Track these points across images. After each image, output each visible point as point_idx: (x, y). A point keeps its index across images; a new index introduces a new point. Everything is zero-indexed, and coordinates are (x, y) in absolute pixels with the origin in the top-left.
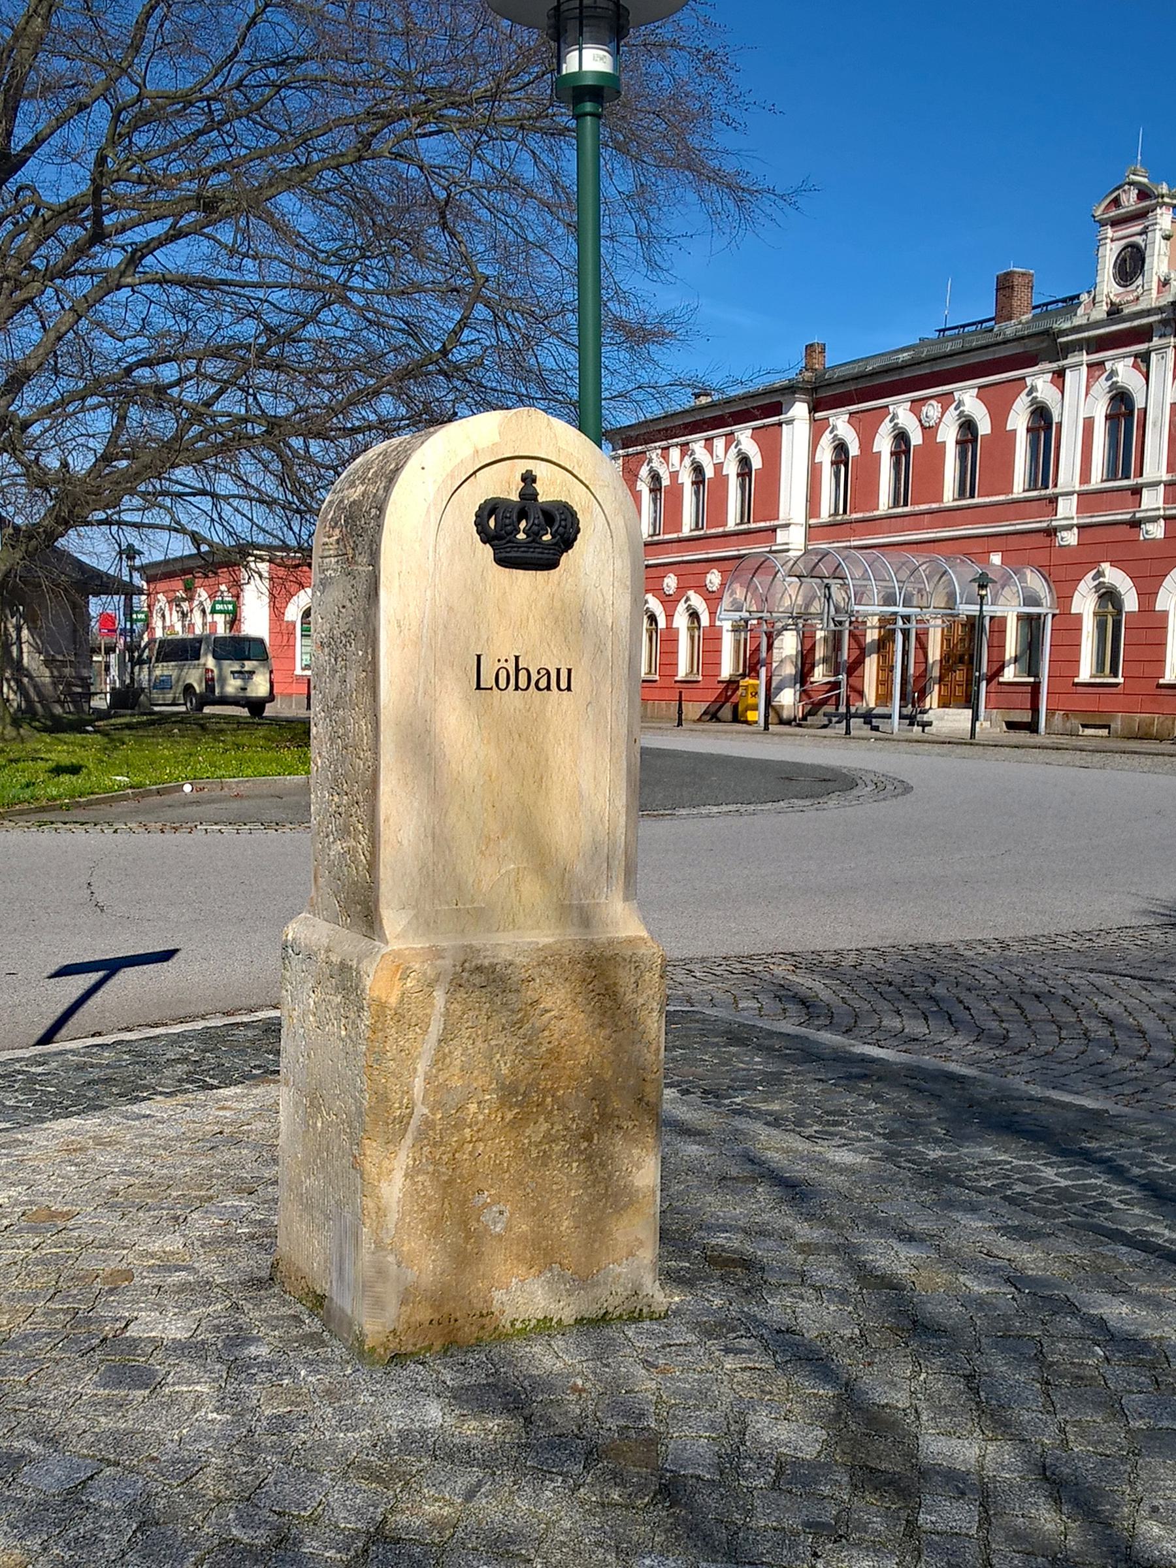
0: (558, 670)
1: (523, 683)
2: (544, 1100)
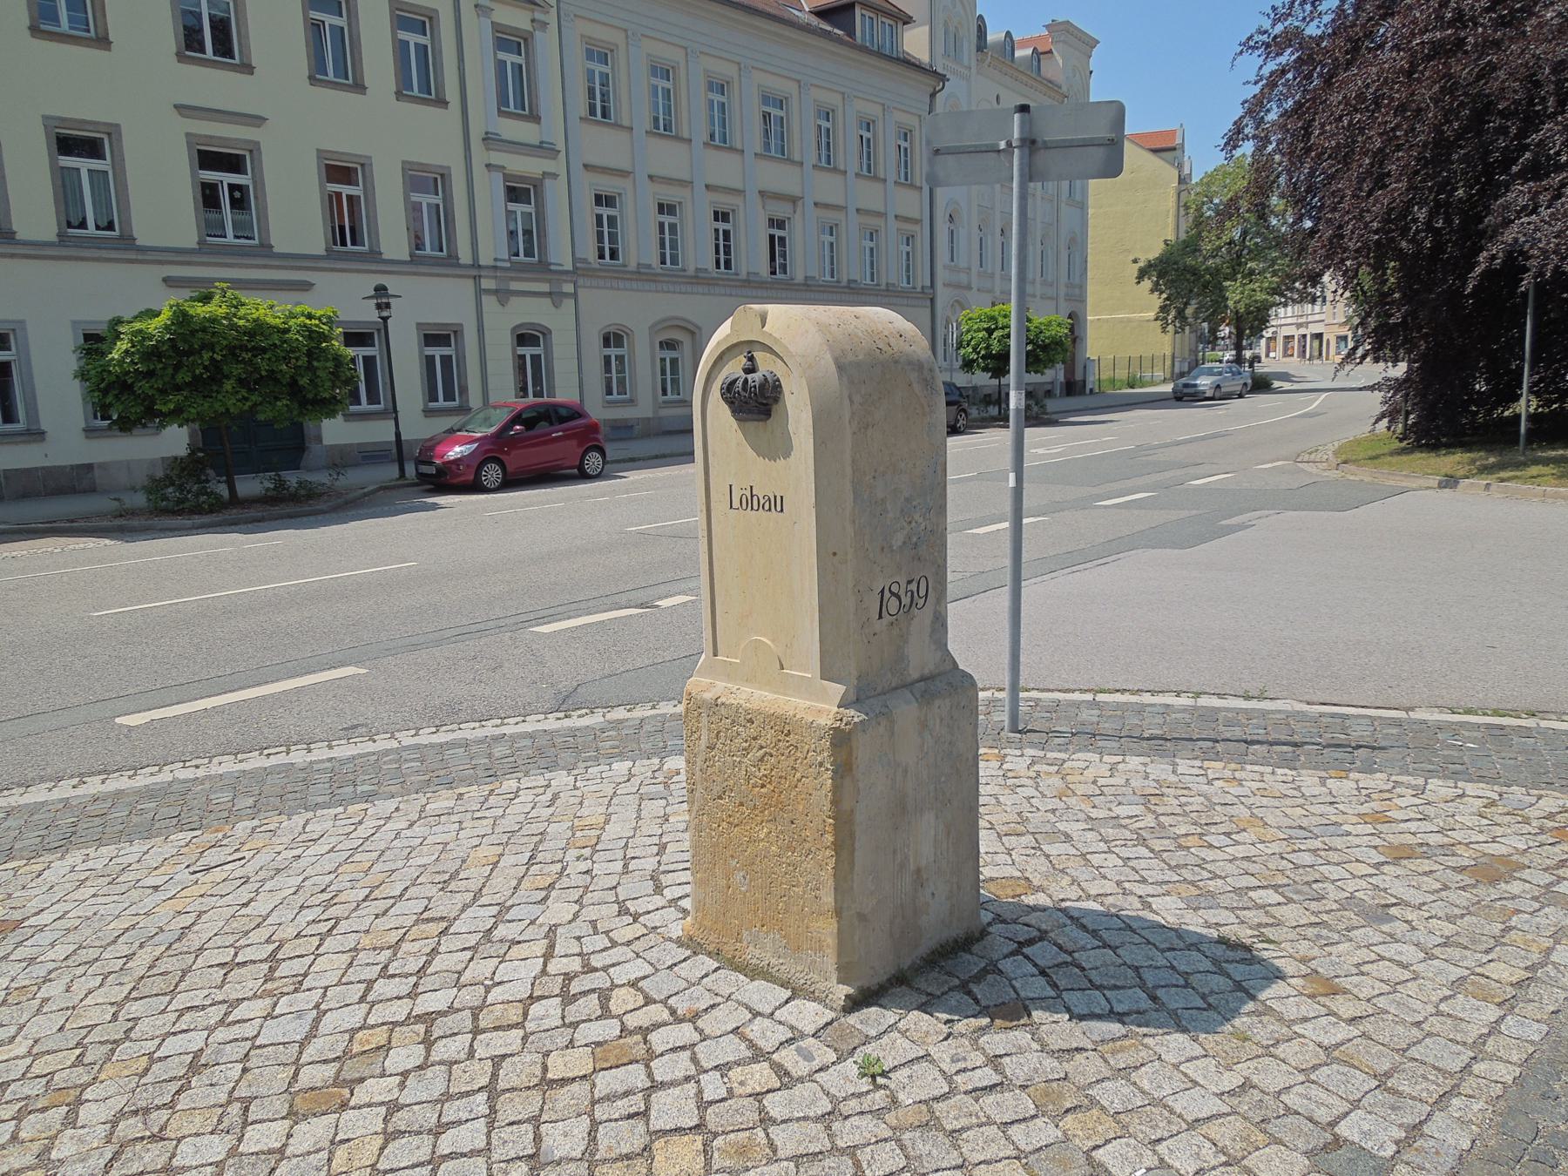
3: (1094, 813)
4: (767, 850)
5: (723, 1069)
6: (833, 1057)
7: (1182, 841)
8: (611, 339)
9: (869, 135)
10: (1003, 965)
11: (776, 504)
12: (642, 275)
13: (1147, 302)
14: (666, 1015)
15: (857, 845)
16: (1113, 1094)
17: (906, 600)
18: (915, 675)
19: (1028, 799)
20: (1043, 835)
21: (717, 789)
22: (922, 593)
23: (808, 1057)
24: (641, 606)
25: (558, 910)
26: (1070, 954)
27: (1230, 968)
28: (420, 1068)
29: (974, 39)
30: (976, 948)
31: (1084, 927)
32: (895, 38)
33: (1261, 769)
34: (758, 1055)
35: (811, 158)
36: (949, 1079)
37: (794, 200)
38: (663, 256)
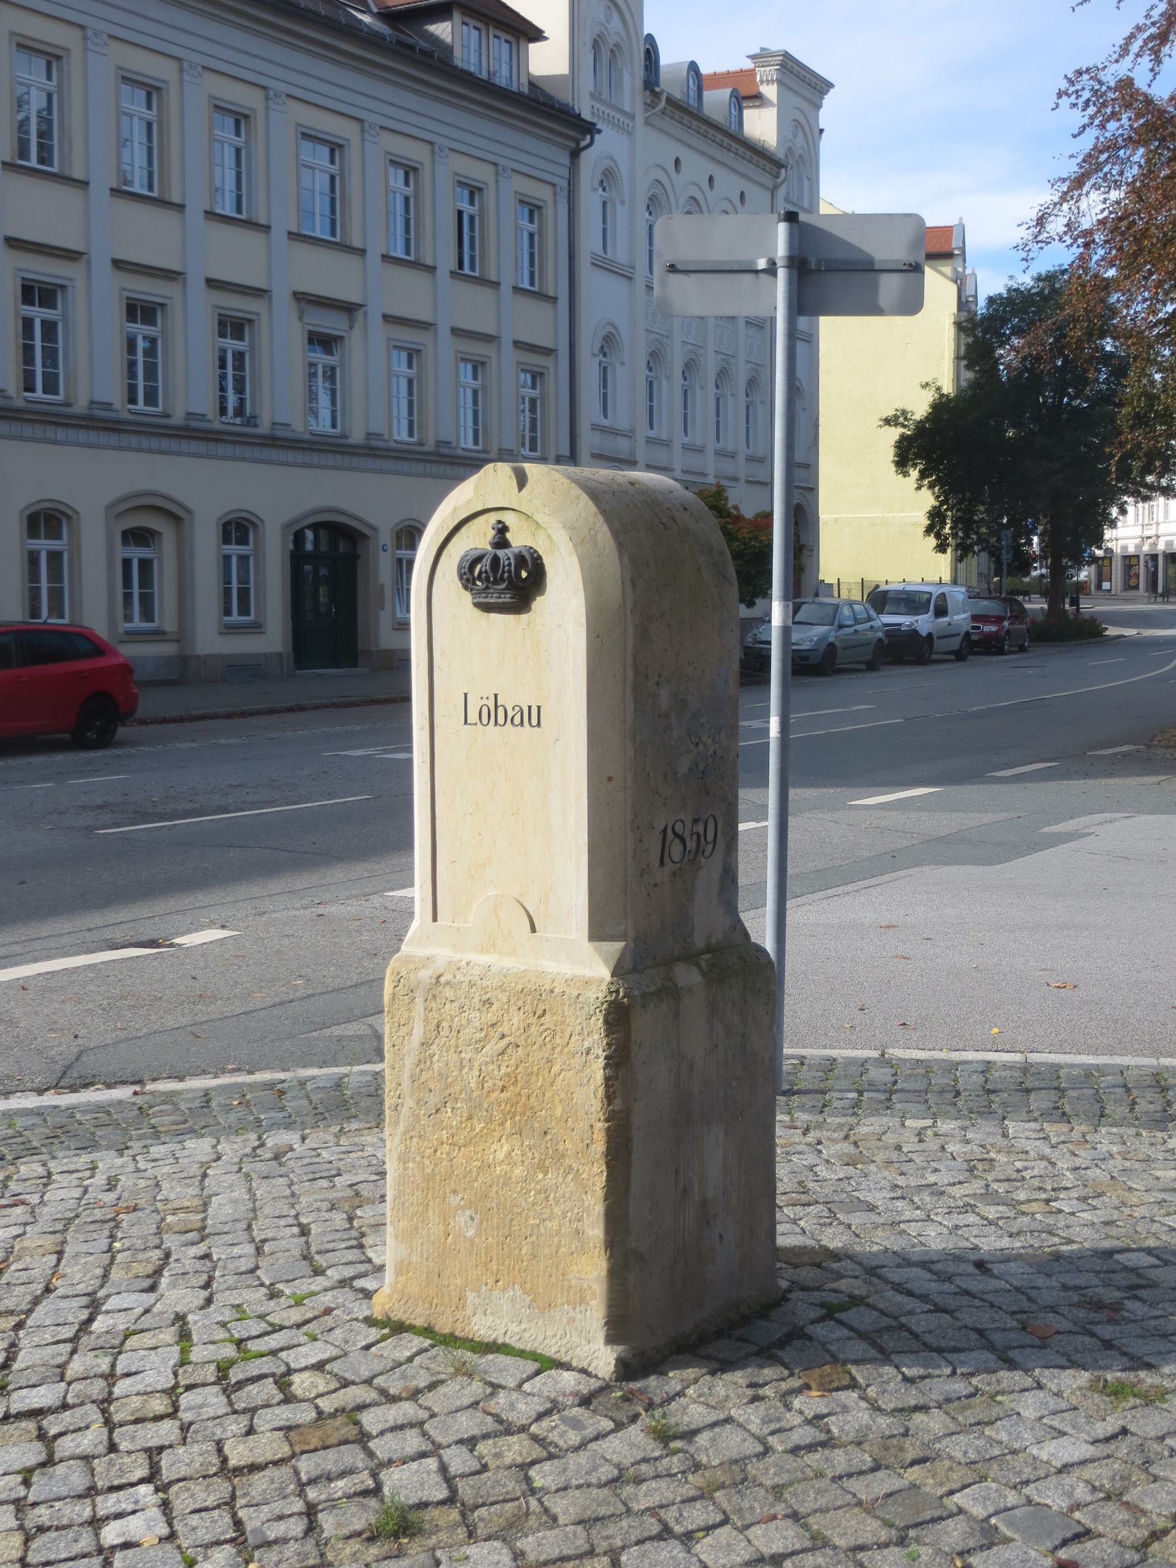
0: (530, 707)
1: (501, 720)
2: (1107, 358)
3: (901, 1181)
4: (507, 1178)
5: (470, 1443)
6: (610, 1425)
7: (1024, 1208)
8: (45, 520)
9: (473, 210)
10: (811, 1330)
11: (531, 717)
12: (98, 424)
13: (915, 499)
14: (374, 1395)
15: (634, 1157)
16: (960, 1447)
17: (691, 845)
18: (700, 942)
19: (811, 1168)
20: (843, 1188)
21: (433, 1100)
22: (710, 837)
23: (576, 1424)
24: (152, 944)
25: (177, 1296)
26: (896, 1319)
27: (1097, 1329)
28: (43, 1465)
29: (640, 72)
30: (774, 1314)
31: (910, 1293)
32: (519, 60)
33: (1122, 1130)
34: (507, 1429)
35: (446, 260)
36: (762, 1440)
37: (349, 309)
38: (132, 389)
